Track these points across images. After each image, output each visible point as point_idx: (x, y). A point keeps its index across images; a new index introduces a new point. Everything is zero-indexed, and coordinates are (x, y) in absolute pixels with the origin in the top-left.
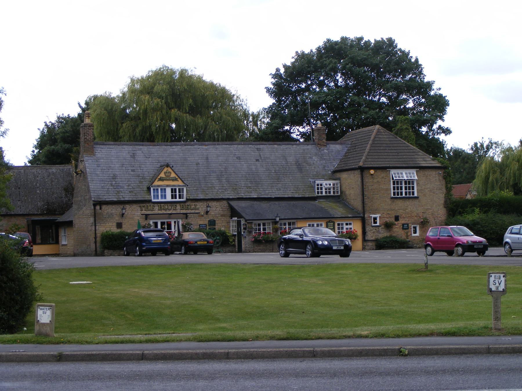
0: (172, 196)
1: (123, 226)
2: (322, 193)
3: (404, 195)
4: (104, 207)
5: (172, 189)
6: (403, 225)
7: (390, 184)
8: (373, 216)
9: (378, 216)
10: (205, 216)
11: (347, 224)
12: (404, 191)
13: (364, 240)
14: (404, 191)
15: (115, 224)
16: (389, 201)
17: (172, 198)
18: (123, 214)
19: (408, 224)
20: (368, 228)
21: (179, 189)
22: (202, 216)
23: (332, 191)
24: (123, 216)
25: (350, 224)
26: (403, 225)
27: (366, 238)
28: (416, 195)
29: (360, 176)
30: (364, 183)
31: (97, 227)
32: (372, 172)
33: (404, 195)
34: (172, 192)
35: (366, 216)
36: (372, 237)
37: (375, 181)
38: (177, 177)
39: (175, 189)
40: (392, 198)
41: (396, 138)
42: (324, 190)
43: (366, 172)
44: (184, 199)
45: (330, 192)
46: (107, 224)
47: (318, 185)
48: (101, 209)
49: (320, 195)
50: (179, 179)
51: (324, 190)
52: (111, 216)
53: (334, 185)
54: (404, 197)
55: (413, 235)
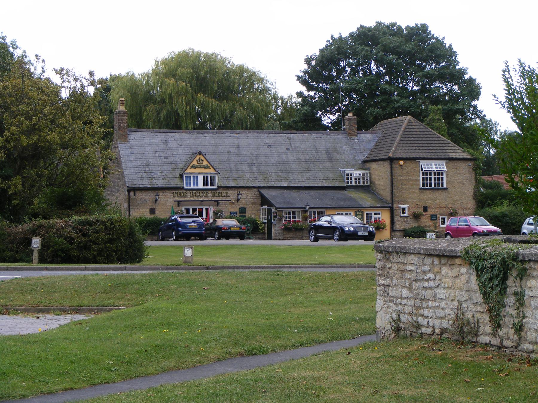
0: (204, 183)
1: (156, 212)
2: (351, 182)
3: (433, 186)
4: (138, 193)
5: (204, 177)
6: (431, 216)
7: (419, 175)
8: (402, 206)
9: (406, 206)
10: (236, 203)
11: (375, 214)
12: (433, 182)
13: (392, 230)
14: (433, 182)
15: (148, 210)
16: (418, 192)
17: (204, 185)
18: (156, 201)
19: (436, 216)
20: (396, 219)
21: (211, 177)
22: (233, 203)
23: (361, 180)
24: (156, 202)
25: (379, 214)
26: (431, 216)
27: (394, 228)
28: (445, 186)
29: (389, 166)
30: (394, 174)
31: (131, 213)
32: (401, 162)
33: (433, 186)
34: (204, 179)
35: (394, 206)
36: (400, 227)
37: (404, 171)
38: (209, 165)
39: (207, 177)
40: (421, 189)
41: (427, 129)
42: (353, 180)
43: (395, 163)
44: (216, 187)
45: (359, 182)
46: (141, 210)
47: (348, 175)
48: (134, 195)
49: (349, 184)
50: (211, 167)
51: (353, 180)
52: (144, 202)
53: (363, 174)
54: (433, 189)
55: (442, 226)
